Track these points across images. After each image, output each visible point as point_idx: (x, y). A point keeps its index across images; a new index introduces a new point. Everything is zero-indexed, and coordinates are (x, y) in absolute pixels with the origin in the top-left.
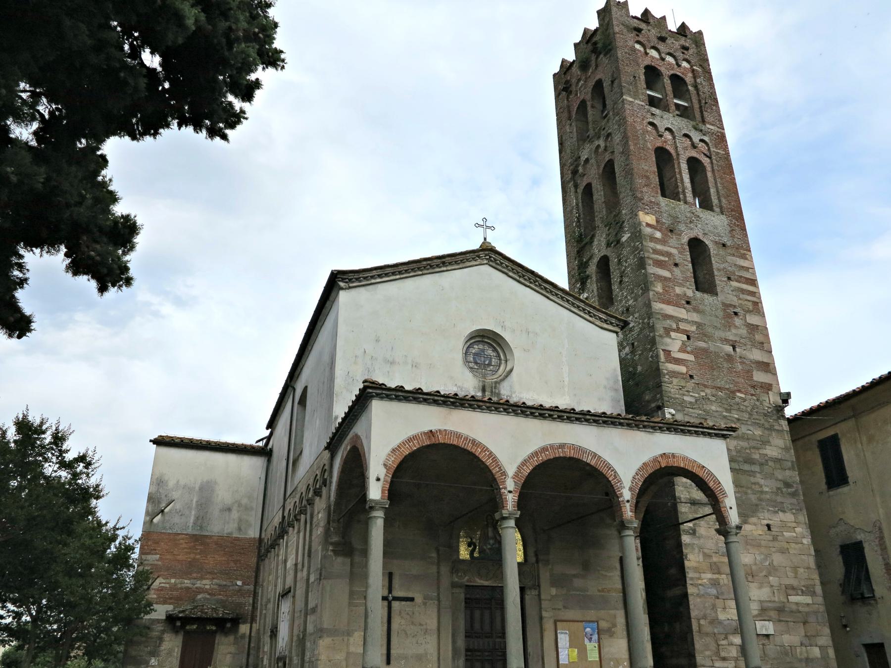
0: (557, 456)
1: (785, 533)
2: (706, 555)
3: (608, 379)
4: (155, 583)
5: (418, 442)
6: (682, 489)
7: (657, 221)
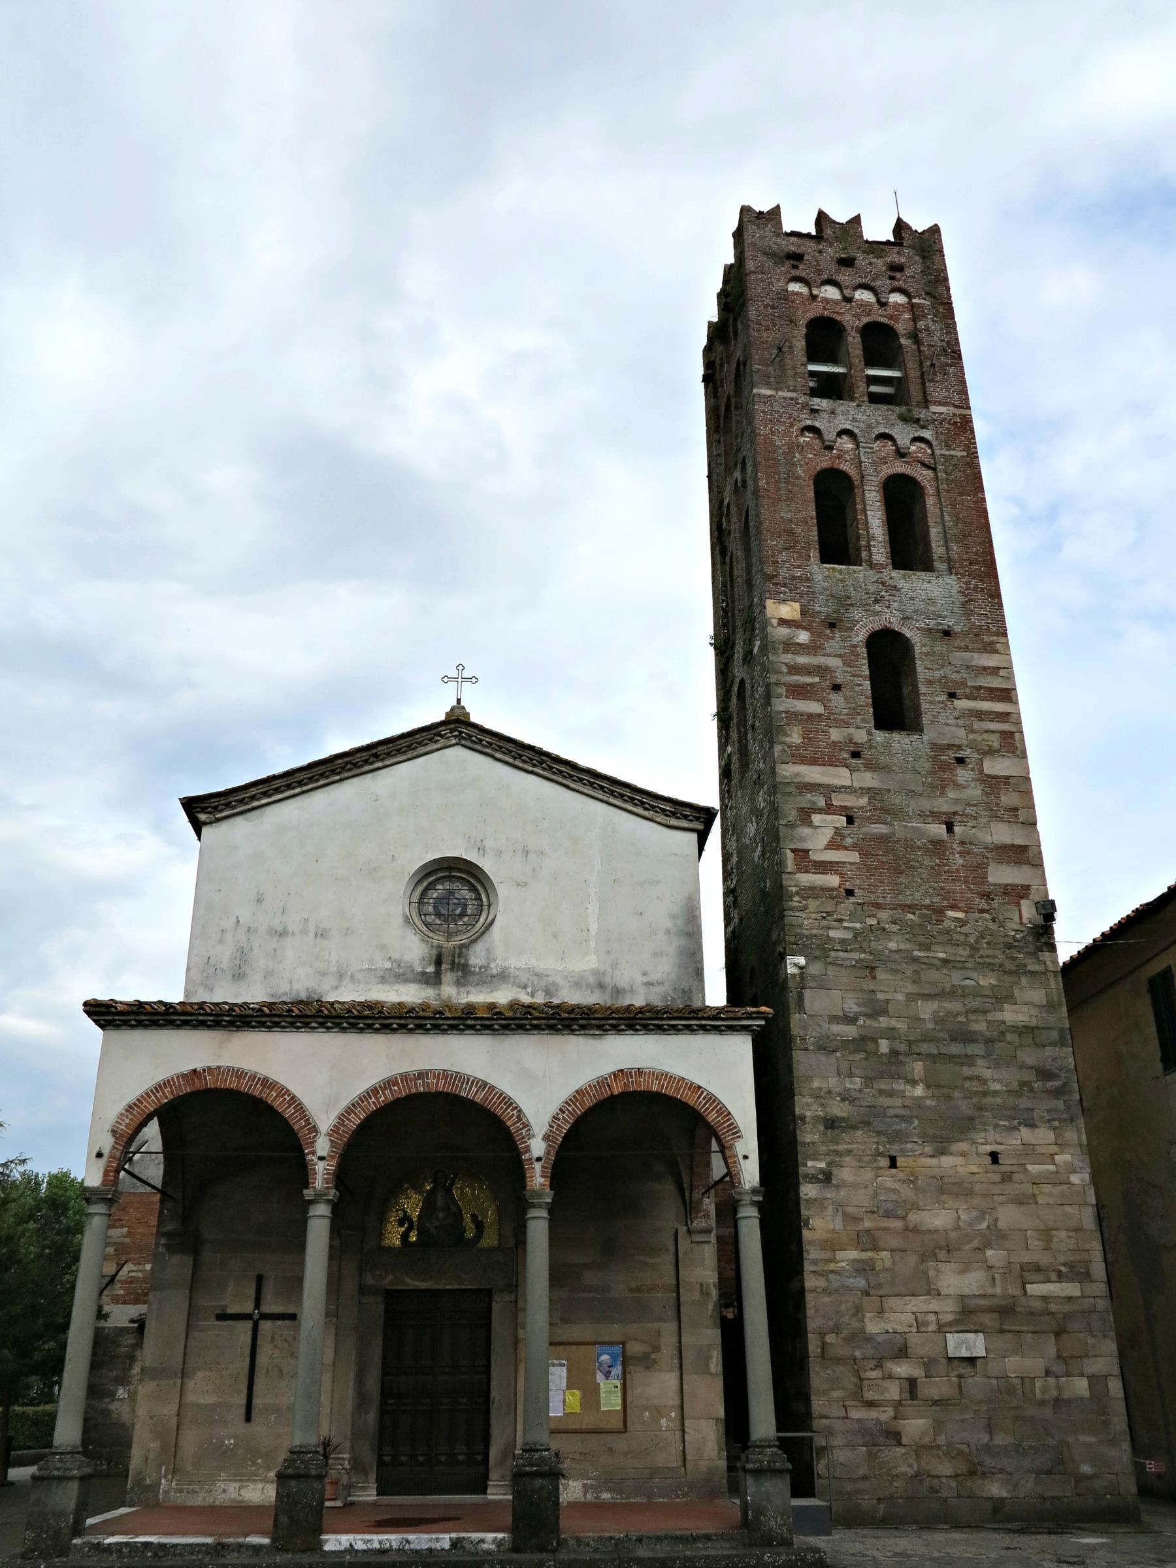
0: (413, 1091)
1: (1029, 1167)
2: (849, 1218)
3: (674, 917)
4: (121, 1272)
5: (172, 1090)
6: (810, 1100)
7: (803, 612)
